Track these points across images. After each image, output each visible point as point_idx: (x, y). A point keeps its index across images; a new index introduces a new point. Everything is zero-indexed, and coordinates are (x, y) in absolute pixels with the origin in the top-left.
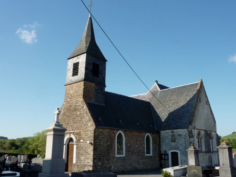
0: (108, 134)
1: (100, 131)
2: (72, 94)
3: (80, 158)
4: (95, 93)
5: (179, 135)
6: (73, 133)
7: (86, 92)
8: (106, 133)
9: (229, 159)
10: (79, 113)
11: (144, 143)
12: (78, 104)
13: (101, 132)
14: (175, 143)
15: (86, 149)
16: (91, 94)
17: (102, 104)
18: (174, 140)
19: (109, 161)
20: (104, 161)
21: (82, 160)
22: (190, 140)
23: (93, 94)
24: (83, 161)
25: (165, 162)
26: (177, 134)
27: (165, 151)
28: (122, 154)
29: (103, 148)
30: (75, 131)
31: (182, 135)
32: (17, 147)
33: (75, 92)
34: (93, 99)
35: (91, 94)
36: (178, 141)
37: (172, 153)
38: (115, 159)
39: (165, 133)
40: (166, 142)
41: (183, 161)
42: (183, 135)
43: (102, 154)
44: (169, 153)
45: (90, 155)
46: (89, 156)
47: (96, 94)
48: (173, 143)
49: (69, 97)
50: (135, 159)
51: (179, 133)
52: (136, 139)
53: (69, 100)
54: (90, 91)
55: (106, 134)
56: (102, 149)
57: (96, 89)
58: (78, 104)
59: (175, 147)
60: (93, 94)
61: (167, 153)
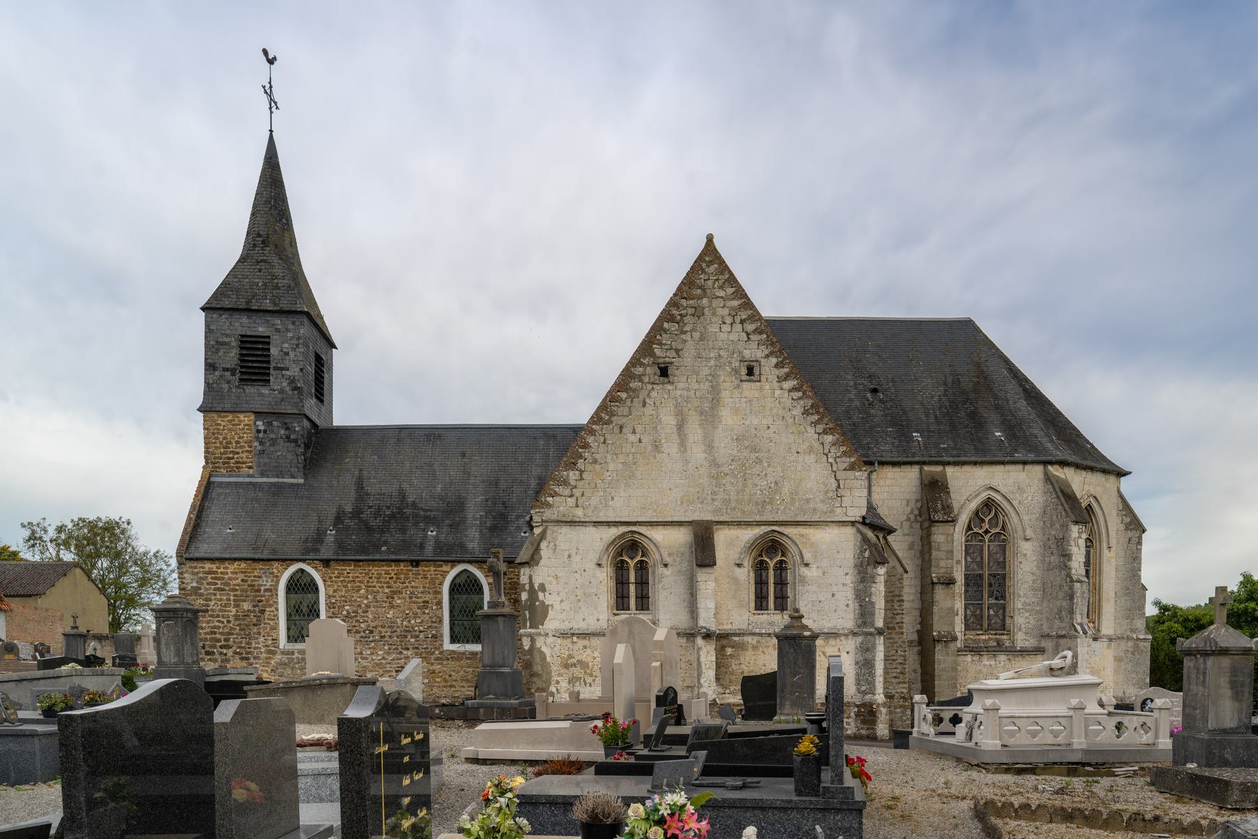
0: (241, 576)
1: (207, 570)
4: (256, 444)
7: (216, 447)
8: (234, 576)
9: (30, 719)
11: (439, 603)
13: (210, 572)
16: (238, 453)
17: (293, 477)
19: (252, 660)
20: (228, 661)
23: (247, 451)
28: (454, 640)
29: (219, 621)
34: (250, 468)
35: (238, 453)
38: (278, 657)
43: (219, 641)
47: (259, 448)
50: (384, 658)
52: (388, 587)
54: (233, 441)
55: (230, 579)
56: (217, 624)
57: (258, 431)
60: (247, 451)
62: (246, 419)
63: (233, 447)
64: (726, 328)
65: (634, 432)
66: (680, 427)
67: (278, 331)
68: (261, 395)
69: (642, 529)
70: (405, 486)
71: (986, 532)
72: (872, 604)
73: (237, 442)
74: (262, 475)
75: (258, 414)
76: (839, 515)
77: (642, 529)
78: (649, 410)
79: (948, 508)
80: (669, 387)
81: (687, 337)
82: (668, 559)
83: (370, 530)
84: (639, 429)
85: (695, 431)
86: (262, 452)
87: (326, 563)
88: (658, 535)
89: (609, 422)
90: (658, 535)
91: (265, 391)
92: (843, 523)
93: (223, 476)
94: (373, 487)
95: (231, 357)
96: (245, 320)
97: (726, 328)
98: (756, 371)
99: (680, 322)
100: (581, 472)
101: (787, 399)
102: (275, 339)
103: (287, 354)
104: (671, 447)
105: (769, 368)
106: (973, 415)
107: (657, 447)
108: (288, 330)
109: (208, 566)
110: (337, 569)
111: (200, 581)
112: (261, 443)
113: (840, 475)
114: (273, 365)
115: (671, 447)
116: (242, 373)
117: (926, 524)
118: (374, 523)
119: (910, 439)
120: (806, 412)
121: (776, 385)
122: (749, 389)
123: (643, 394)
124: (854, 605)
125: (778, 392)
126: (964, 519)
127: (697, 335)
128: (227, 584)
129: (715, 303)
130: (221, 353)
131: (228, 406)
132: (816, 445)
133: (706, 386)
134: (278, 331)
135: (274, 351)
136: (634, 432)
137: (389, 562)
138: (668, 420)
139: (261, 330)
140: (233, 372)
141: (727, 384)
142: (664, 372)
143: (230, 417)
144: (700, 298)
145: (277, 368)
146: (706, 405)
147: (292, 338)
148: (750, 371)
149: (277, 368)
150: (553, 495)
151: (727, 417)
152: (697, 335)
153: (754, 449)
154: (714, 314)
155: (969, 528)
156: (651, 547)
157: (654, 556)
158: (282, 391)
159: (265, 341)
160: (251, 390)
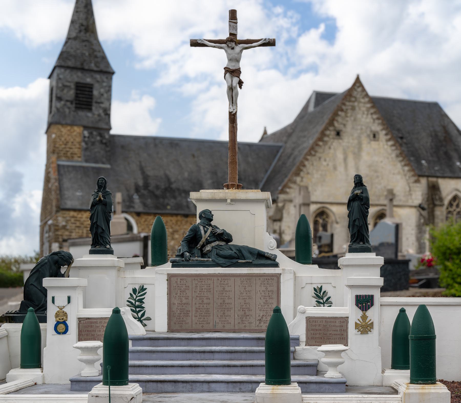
13: (73, 217)
34: (79, 157)
55: (84, 221)
57: (85, 137)
62: (78, 130)
63: (69, 145)
64: (365, 116)
65: (325, 160)
66: (345, 159)
67: (98, 82)
68: (87, 117)
69: (328, 206)
70: (168, 172)
71: (455, 210)
72: (424, 243)
73: (72, 142)
74: (87, 161)
75: (85, 128)
76: (410, 203)
77: (328, 206)
78: (332, 151)
79: (441, 199)
80: (340, 141)
81: (348, 119)
82: (338, 220)
83: (156, 197)
84: (328, 159)
85: (351, 162)
86: (86, 149)
87: (138, 214)
88: (334, 209)
89: (314, 155)
90: (334, 209)
91: (90, 115)
92: (411, 207)
93: (63, 161)
94: (150, 173)
95: (71, 94)
96: (79, 74)
97: (365, 116)
98: (377, 136)
99: (346, 112)
100: (302, 178)
101: (389, 150)
102: (96, 86)
103: (102, 95)
104: (341, 169)
105: (382, 135)
106: (446, 153)
107: (335, 168)
108: (103, 82)
109: (72, 213)
110: (144, 218)
111: (67, 221)
112: (86, 143)
113: (411, 185)
114: (94, 100)
115: (341, 169)
116: (76, 104)
117: (431, 206)
118: (158, 193)
119: (421, 165)
120: (397, 156)
121: (385, 143)
122: (374, 144)
123: (329, 144)
124: (416, 244)
125: (386, 147)
126: (446, 202)
127: (352, 118)
128: (82, 224)
129: (361, 105)
130: (65, 91)
131: (69, 122)
132: (401, 171)
133: (356, 142)
134: (98, 82)
135: (95, 93)
136: (325, 160)
137: (172, 215)
138: (340, 156)
139: (89, 80)
140: (72, 102)
141: (365, 141)
142: (338, 134)
143: (69, 128)
144: (354, 102)
145: (97, 102)
146: (356, 150)
147: (106, 86)
148: (374, 136)
149: (97, 102)
150: (290, 188)
151: (365, 157)
152: (352, 118)
153: (376, 171)
154: (360, 109)
155: (447, 208)
156: (331, 214)
157: (332, 218)
158: (99, 115)
159: (90, 87)
160: (81, 113)
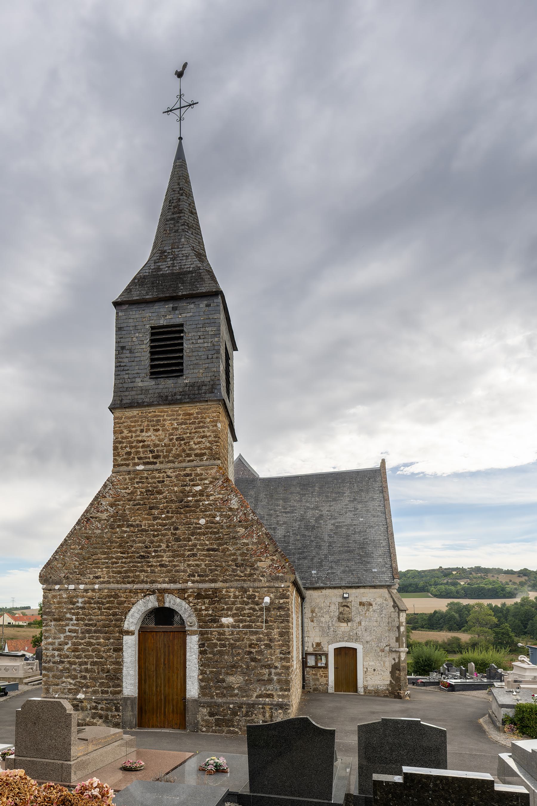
2: (158, 446)
3: (223, 681)
5: (361, 604)
6: (181, 593)
10: (202, 521)
12: (198, 488)
14: (349, 624)
15: (253, 650)
18: (343, 618)
21: (234, 689)
22: (399, 618)
24: (236, 691)
25: (316, 675)
26: (359, 600)
27: (318, 644)
30: (190, 584)
31: (372, 605)
32: (424, 670)
33: (171, 440)
36: (357, 619)
37: (338, 651)
39: (319, 596)
40: (323, 619)
41: (370, 670)
42: (374, 604)
44: (330, 650)
45: (273, 671)
46: (270, 674)
48: (344, 625)
49: (139, 458)
51: (364, 600)
53: (141, 467)
58: (198, 488)
59: (350, 635)
61: (325, 649)
